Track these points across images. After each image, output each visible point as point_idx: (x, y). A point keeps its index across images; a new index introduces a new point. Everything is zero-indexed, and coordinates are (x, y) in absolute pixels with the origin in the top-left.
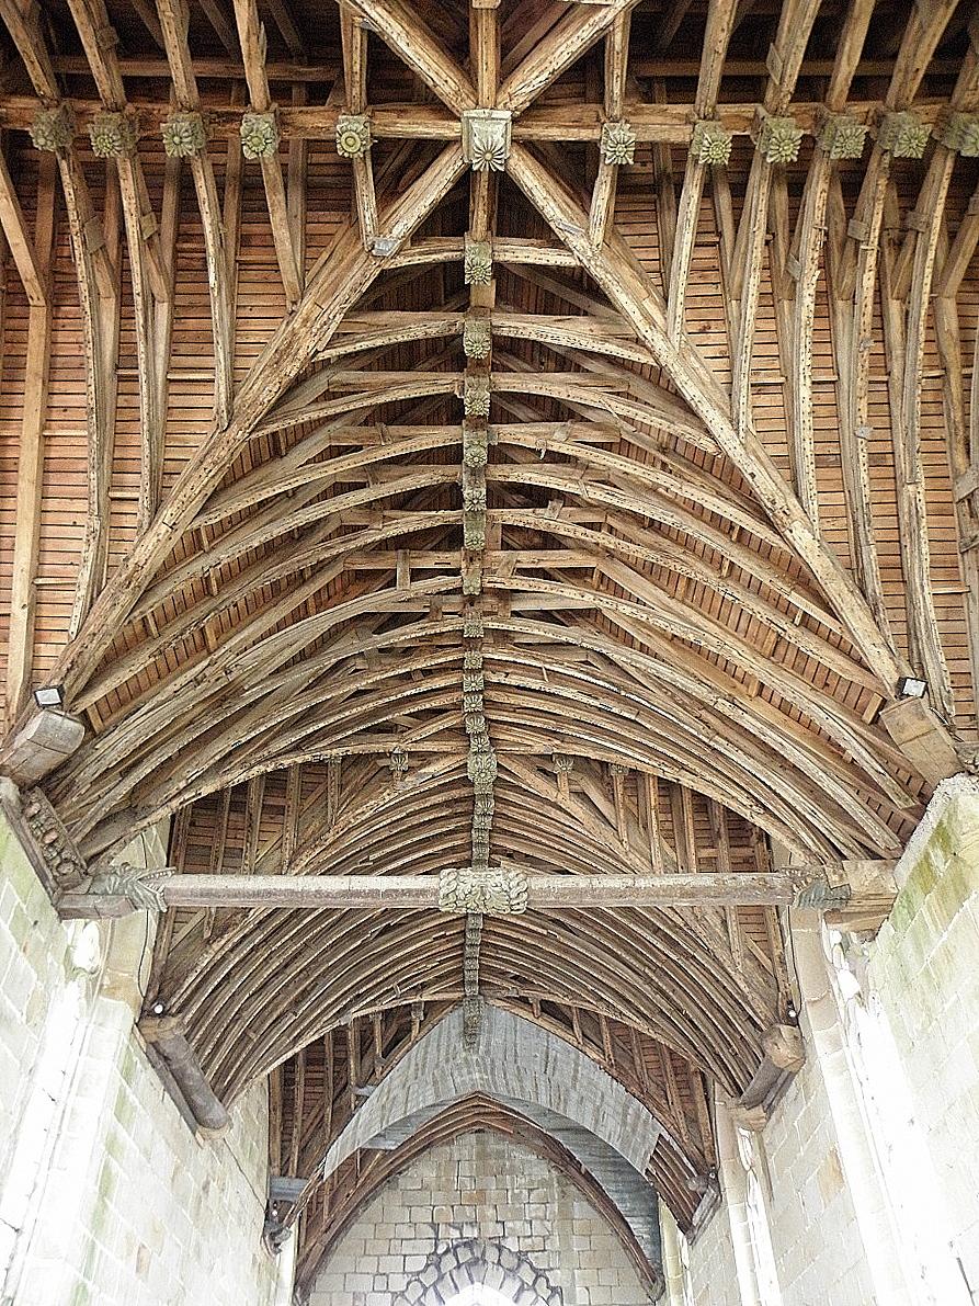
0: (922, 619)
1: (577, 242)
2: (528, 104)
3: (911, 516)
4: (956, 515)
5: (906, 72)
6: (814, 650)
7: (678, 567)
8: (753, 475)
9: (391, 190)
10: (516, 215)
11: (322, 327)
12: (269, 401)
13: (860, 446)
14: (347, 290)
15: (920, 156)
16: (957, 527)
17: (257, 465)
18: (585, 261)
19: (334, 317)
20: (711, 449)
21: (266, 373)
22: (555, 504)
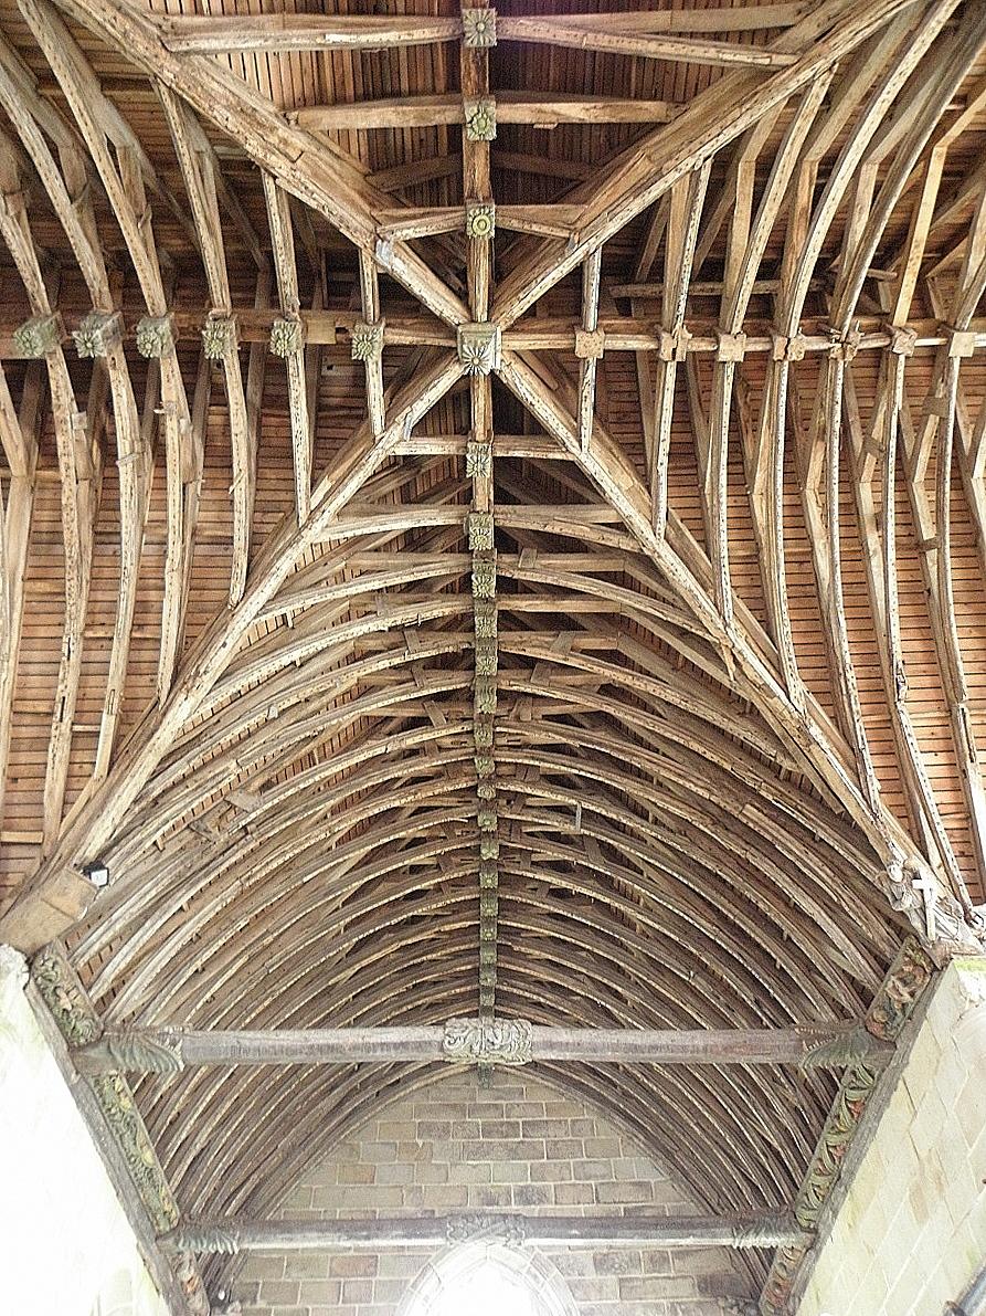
0: (139, 837)
1: (396, 432)
2: (505, 382)
3: (213, 778)
4: (215, 804)
5: (521, 643)
6: (57, 759)
7: (73, 583)
8: (224, 645)
9: (427, 249)
10: (404, 371)
11: (303, 184)
12: (215, 118)
13: (261, 715)
14: (341, 212)
15: (80, 356)
16: (206, 810)
17: (89, 56)
18: (380, 445)
19: (314, 199)
20: (235, 597)
21: (231, 98)
22: (85, 419)
